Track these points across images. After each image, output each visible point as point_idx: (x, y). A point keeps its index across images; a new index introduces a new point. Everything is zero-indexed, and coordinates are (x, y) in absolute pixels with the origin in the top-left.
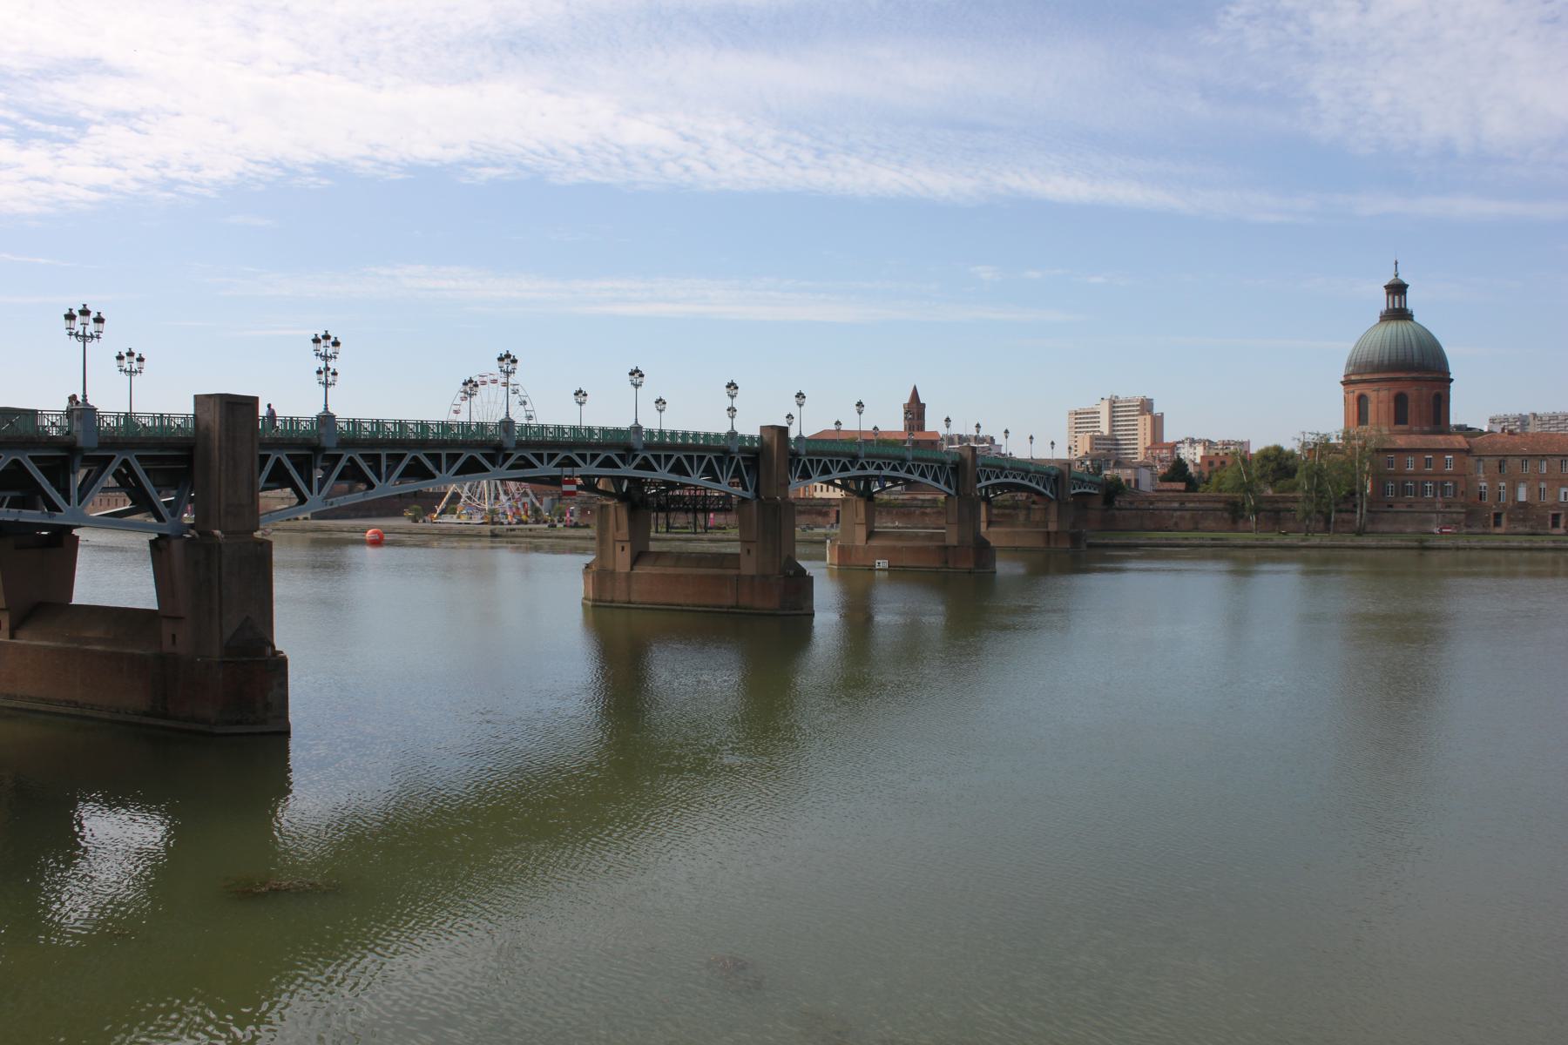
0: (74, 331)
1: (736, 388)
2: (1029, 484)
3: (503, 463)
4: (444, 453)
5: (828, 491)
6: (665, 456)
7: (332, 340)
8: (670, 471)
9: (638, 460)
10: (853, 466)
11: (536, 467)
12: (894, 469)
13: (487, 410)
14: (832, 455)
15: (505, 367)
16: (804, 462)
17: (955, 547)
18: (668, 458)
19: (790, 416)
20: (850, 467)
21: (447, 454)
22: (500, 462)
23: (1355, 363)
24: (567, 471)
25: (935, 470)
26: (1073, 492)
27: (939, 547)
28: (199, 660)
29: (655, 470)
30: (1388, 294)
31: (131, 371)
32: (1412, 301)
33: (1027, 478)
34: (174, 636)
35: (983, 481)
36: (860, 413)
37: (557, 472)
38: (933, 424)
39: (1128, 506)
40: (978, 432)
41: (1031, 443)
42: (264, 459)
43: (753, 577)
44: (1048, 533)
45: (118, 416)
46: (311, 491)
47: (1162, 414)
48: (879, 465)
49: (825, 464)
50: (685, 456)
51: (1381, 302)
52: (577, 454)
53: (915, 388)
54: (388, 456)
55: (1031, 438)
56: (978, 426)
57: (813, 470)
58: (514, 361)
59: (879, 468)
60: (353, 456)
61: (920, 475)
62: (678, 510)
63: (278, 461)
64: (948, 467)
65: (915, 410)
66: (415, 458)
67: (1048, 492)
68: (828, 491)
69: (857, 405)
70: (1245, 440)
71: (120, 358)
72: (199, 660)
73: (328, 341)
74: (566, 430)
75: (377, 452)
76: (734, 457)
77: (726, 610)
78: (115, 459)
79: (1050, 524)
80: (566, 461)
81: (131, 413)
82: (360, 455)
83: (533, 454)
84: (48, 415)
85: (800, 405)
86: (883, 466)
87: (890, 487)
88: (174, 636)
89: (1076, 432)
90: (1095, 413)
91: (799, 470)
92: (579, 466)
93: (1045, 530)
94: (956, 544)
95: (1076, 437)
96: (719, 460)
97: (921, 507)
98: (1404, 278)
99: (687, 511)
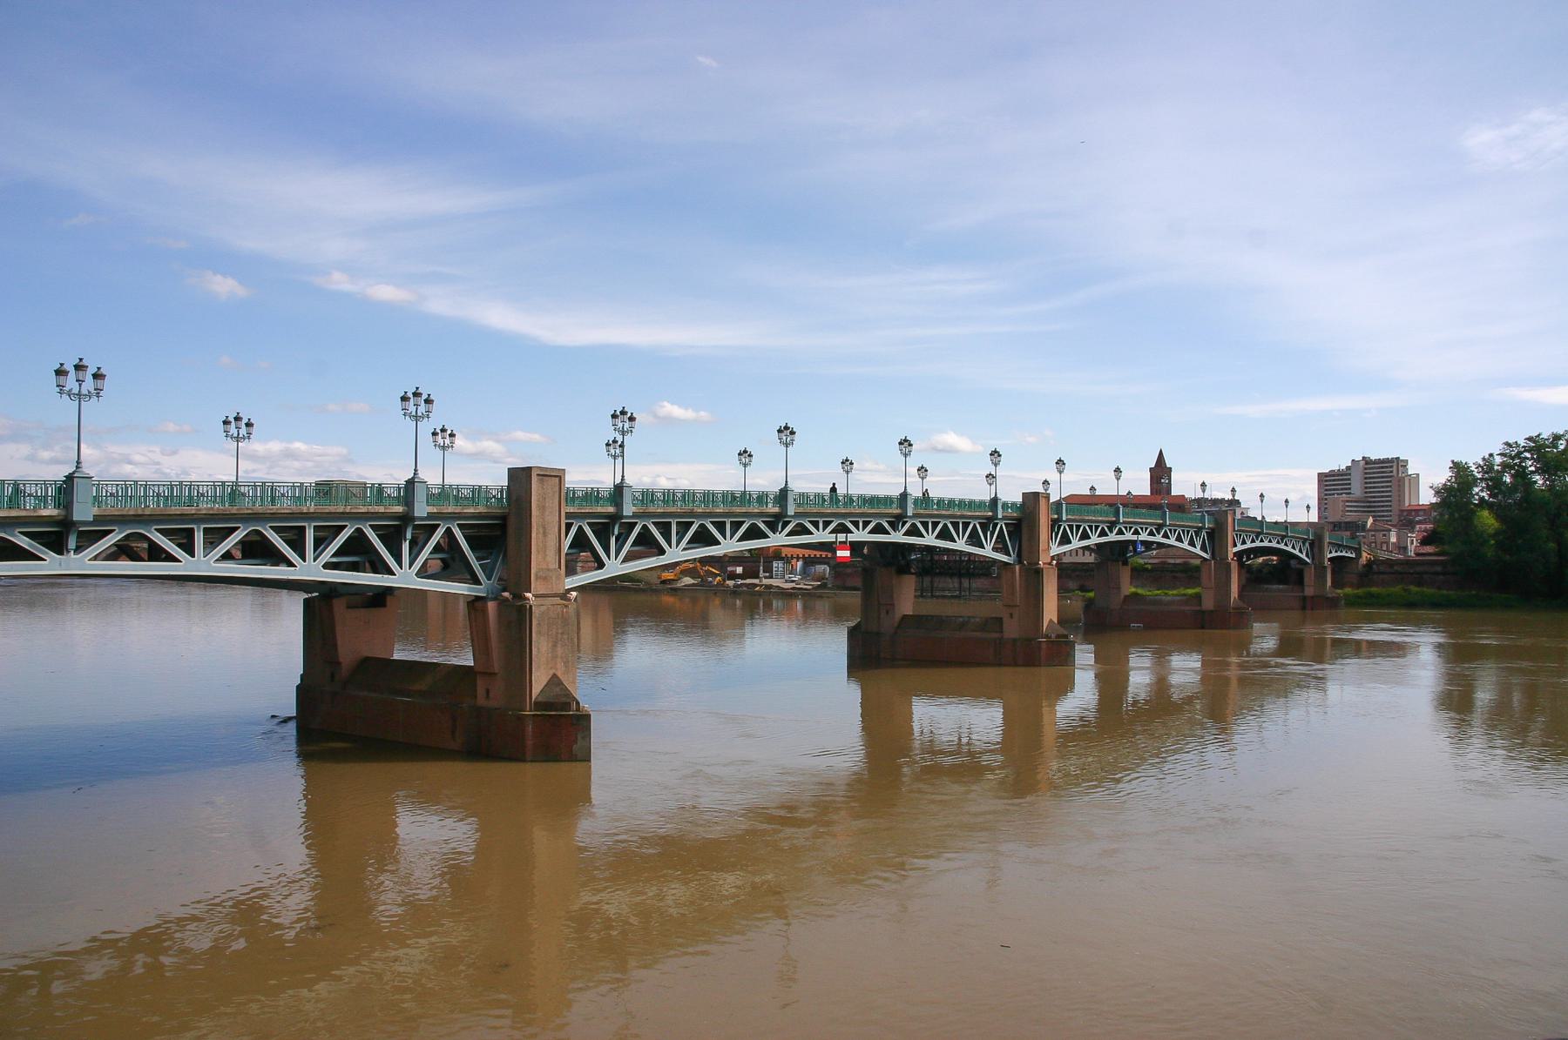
0: (66, 389)
4: (930, 521)
5: (1084, 555)
7: (629, 415)
8: (937, 538)
9: (907, 526)
11: (719, 543)
12: (1151, 534)
13: (763, 479)
17: (1212, 611)
18: (935, 525)
19: (1046, 483)
22: (780, 530)
24: (841, 537)
26: (1329, 556)
28: (510, 713)
31: (79, 394)
34: (488, 692)
36: (1118, 479)
37: (831, 538)
40: (1234, 496)
41: (1287, 507)
42: (569, 526)
43: (1014, 640)
46: (928, 533)
48: (1136, 530)
49: (1136, 530)
54: (963, 523)
57: (959, 537)
58: (793, 433)
61: (1176, 540)
62: (941, 574)
63: (1103, 528)
64: (1001, 524)
65: (1160, 472)
66: (702, 526)
67: (1303, 556)
68: (1084, 555)
69: (1115, 471)
72: (510, 713)
75: (190, 526)
79: (1306, 589)
80: (799, 529)
81: (745, 491)
84: (107, 485)
85: (1061, 472)
86: (1124, 529)
88: (488, 692)
89: (1326, 495)
90: (1346, 475)
91: (1059, 536)
93: (1301, 594)
95: (1326, 499)
97: (1172, 571)
99: (952, 575)
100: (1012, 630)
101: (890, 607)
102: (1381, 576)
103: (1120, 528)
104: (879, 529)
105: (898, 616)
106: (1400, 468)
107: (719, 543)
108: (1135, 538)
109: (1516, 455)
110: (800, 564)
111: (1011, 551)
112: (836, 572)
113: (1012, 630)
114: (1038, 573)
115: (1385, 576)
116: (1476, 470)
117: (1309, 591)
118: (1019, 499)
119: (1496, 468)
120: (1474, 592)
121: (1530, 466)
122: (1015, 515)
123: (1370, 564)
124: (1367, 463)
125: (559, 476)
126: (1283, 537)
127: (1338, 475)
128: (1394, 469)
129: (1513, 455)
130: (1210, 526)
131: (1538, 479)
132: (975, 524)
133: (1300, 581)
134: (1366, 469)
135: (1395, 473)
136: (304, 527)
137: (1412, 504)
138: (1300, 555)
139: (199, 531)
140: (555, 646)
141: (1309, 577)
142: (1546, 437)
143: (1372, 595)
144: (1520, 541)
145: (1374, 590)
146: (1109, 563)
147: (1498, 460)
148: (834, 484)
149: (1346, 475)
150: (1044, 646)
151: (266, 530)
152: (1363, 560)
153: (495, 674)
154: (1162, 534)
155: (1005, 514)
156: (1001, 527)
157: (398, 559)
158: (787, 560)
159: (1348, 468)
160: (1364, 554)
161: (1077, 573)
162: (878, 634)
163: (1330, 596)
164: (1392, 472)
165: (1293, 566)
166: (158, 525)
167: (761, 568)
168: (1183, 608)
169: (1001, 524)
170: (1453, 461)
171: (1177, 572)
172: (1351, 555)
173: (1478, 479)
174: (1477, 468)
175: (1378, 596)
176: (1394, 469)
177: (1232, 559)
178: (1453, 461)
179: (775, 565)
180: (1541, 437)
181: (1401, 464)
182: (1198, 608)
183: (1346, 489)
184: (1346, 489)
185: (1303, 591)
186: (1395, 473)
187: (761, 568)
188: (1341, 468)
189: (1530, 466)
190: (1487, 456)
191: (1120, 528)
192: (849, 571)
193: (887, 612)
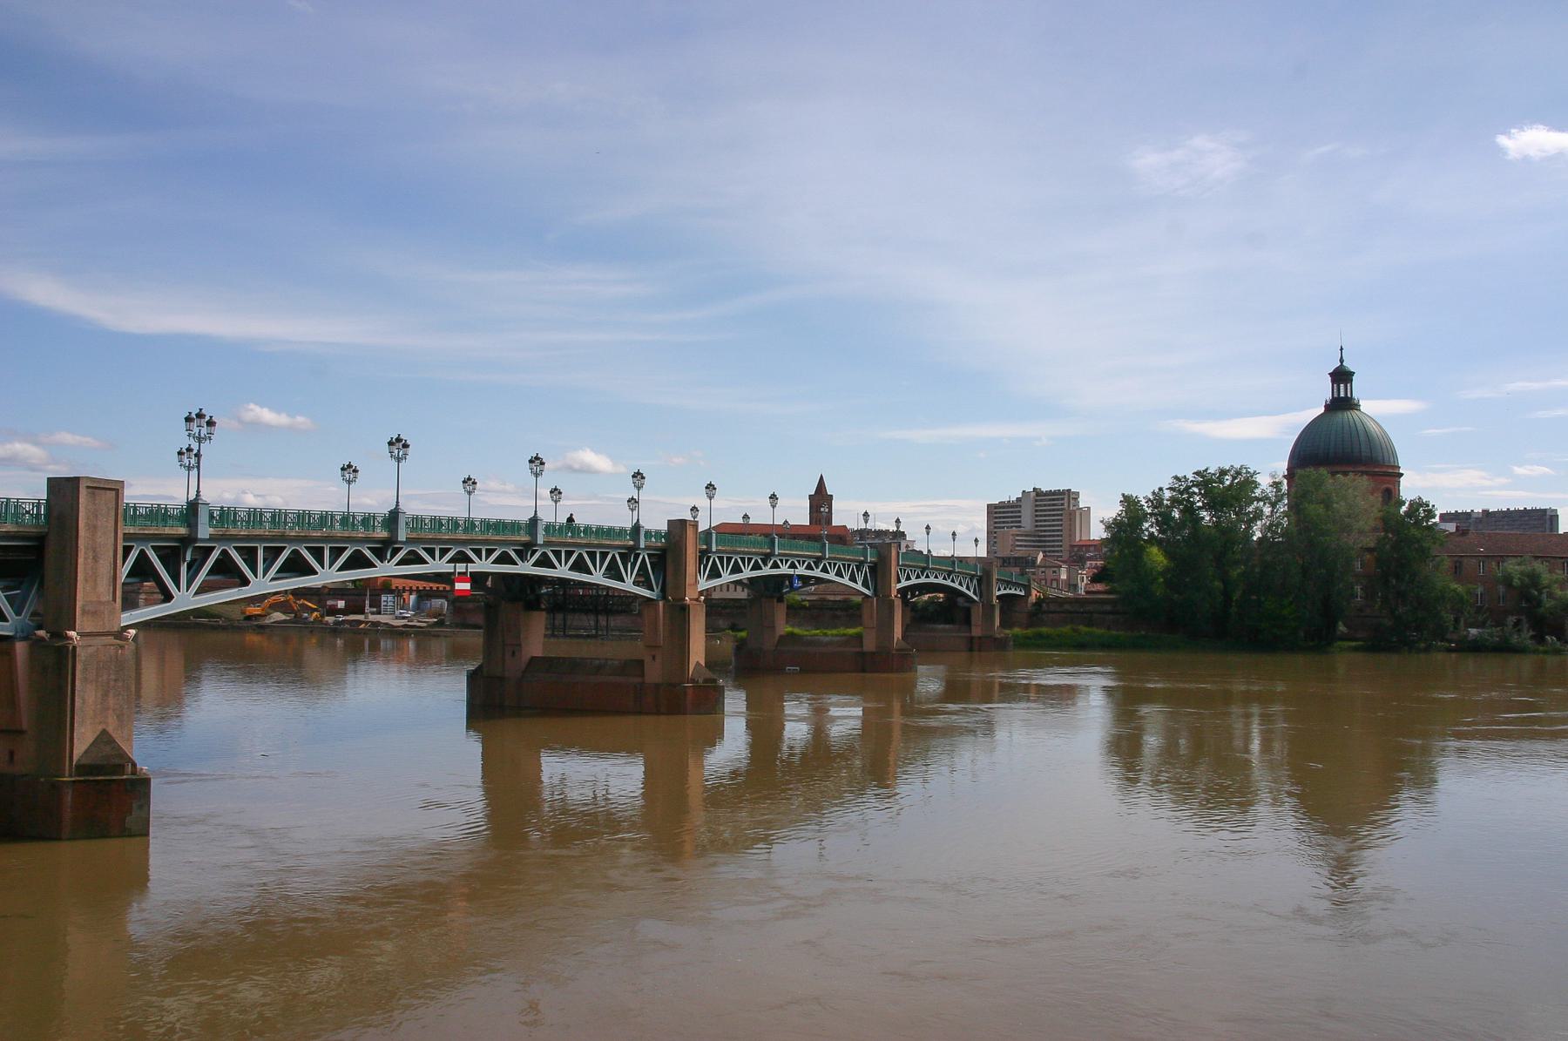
1: (643, 478)
2: (952, 584)
3: (392, 557)
4: (746, 557)
6: (487, 549)
7: (207, 418)
11: (316, 573)
15: (396, 451)
18: (569, 554)
19: (694, 509)
20: (762, 566)
21: (264, 547)
22: (388, 558)
24: (461, 567)
26: (998, 593)
27: (858, 653)
28: (42, 780)
30: (1333, 382)
32: (1358, 389)
34: (12, 754)
35: (903, 581)
36: (774, 507)
37: (449, 568)
42: (127, 550)
43: (657, 686)
44: (972, 638)
45: (39, 503)
47: (1089, 508)
51: (1325, 392)
53: (822, 476)
56: (898, 521)
57: (596, 569)
59: (793, 566)
60: (144, 548)
62: (574, 611)
64: (644, 555)
66: (295, 552)
67: (971, 594)
71: (180, 453)
72: (42, 780)
73: (202, 420)
74: (477, 523)
77: (192, 778)
79: (973, 628)
82: (551, 551)
86: (779, 562)
87: (800, 587)
90: (1017, 506)
91: (637, 568)
92: (473, 562)
93: (968, 634)
94: (874, 650)
95: (995, 533)
96: (624, 558)
98: (1349, 365)
99: (587, 612)
100: (654, 673)
101: (516, 648)
102: (1050, 615)
103: (775, 561)
104: (504, 559)
106: (1072, 501)
108: (791, 572)
114: (684, 609)
116: (1146, 505)
117: (976, 632)
118: (664, 527)
119: (1165, 502)
120: (1143, 633)
121: (1198, 501)
123: (1039, 602)
124: (1037, 495)
125: (116, 488)
126: (950, 573)
128: (1066, 499)
129: (1182, 490)
134: (1036, 501)
136: (323, 547)
138: (967, 592)
139: (137, 549)
140: (106, 695)
141: (977, 615)
143: (1040, 636)
145: (1044, 630)
147: (1167, 494)
148: (571, 515)
149: (1017, 506)
150: (690, 692)
151: (230, 549)
152: (1033, 599)
153: (22, 732)
154: (821, 567)
157: (255, 572)
158: (398, 593)
159: (1019, 500)
160: (1034, 592)
161: (728, 611)
163: (998, 636)
164: (1062, 504)
167: (367, 602)
170: (1123, 495)
171: (836, 609)
174: (1146, 502)
175: (1048, 636)
177: (896, 596)
178: (1123, 495)
179: (384, 598)
180: (1209, 471)
181: (1072, 496)
182: (858, 650)
183: (1016, 522)
184: (1016, 522)
187: (367, 602)
189: (1198, 501)
190: (1157, 491)
191: (775, 561)
192: (471, 606)
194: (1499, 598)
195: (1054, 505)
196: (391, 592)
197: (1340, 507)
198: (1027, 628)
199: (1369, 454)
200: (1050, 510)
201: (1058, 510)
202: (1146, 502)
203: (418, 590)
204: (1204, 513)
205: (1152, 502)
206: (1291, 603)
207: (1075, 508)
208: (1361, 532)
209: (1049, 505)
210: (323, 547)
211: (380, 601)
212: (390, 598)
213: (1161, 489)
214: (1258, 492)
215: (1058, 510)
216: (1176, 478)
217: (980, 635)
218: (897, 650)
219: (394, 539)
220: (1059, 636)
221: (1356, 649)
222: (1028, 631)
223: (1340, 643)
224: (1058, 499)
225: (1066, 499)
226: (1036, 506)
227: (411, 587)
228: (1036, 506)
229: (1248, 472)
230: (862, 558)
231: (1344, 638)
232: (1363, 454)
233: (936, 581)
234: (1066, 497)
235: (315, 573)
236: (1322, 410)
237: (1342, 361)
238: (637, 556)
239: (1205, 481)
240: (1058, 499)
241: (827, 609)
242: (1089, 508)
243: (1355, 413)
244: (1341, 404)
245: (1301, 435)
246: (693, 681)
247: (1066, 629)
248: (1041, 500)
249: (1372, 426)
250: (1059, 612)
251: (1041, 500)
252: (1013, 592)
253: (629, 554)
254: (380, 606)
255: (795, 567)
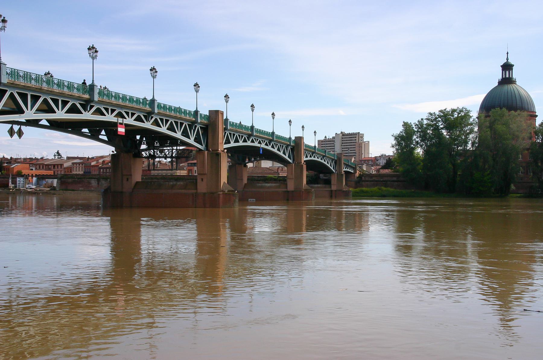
3: (90, 109)
7: (2, 18)
10: (147, 120)
11: (247, 142)
14: (281, 144)
16: (237, 135)
17: (293, 191)
22: (88, 109)
23: (485, 107)
24: (120, 120)
25: (284, 148)
27: (286, 191)
29: (55, 112)
30: (503, 70)
32: (516, 74)
33: (249, 140)
37: (115, 120)
38: (328, 138)
39: (370, 179)
43: (204, 194)
44: (332, 191)
47: (369, 142)
50: (160, 118)
51: (498, 75)
52: (104, 108)
55: (303, 127)
58: (96, 52)
60: (12, 92)
63: (245, 137)
64: (198, 126)
70: (501, 67)
76: (226, 132)
78: (41, 97)
79: (332, 186)
83: (51, 98)
92: (126, 118)
93: (330, 189)
94: (293, 190)
98: (511, 61)
100: (202, 187)
101: (129, 176)
102: (366, 183)
105: (134, 182)
106: (360, 138)
107: (247, 142)
108: (259, 145)
109: (434, 120)
110: (35, 179)
111: (203, 143)
112: (61, 181)
113: (202, 187)
114: (218, 155)
115: (368, 182)
116: (415, 127)
117: (334, 188)
119: (424, 126)
120: (413, 190)
121: (441, 125)
122: (206, 122)
123: (360, 176)
124: (343, 135)
126: (324, 156)
127: (329, 141)
128: (357, 137)
129: (433, 118)
130: (293, 145)
131: (444, 132)
132: (186, 125)
133: (328, 182)
135: (357, 141)
137: (365, 157)
139: (9, 92)
141: (334, 179)
142: (448, 111)
143: (363, 191)
144: (435, 164)
145: (364, 189)
146: (237, 165)
147: (425, 122)
149: (332, 141)
150: (221, 196)
152: (357, 174)
155: (201, 121)
156: (227, 134)
158: (26, 177)
159: (334, 138)
160: (358, 172)
162: (122, 192)
163: (344, 190)
164: (356, 140)
165: (321, 178)
166: (112, 107)
167: (10, 180)
168: (277, 190)
169: (198, 126)
170: (404, 122)
172: (351, 171)
173: (416, 131)
174: (415, 126)
175: (366, 192)
176: (357, 139)
177: (303, 163)
178: (404, 122)
179: (18, 179)
180: (446, 110)
181: (360, 136)
182: (286, 190)
183: (332, 149)
184: (332, 149)
185: (331, 187)
186: (357, 141)
187: (10, 180)
188: (330, 138)
189: (441, 125)
190: (420, 120)
192: (70, 180)
193: (128, 180)
194: (467, 259)
195: (351, 140)
196: (22, 176)
197: (513, 126)
198: (355, 188)
199: (521, 106)
200: (349, 143)
201: (353, 143)
202: (415, 126)
203: (36, 176)
204: (443, 131)
205: (418, 125)
206: (489, 174)
207: (362, 142)
208: (524, 139)
209: (349, 140)
210: (27, 94)
211: (16, 182)
212: (22, 179)
213: (422, 119)
214: (471, 120)
215: (353, 143)
216: (431, 114)
217: (336, 189)
218: (304, 190)
219: (153, 112)
220: (371, 191)
221: (520, 197)
222: (356, 190)
223: (511, 195)
224: (353, 137)
225: (357, 137)
226: (343, 141)
227: (32, 174)
228: (343, 141)
229: (466, 110)
230: (289, 143)
231: (514, 192)
232: (518, 106)
233: (318, 160)
234: (357, 136)
235: (55, 112)
236: (497, 84)
237: (507, 59)
238: (196, 126)
239: (445, 115)
240: (353, 137)
241: (256, 180)
242: (369, 142)
243: (513, 86)
244: (506, 81)
245: (489, 92)
246: (223, 191)
247: (375, 189)
248: (345, 138)
249: (522, 92)
250: (371, 181)
251: (345, 138)
252: (348, 170)
253: (192, 125)
254: (16, 184)
255: (261, 143)
